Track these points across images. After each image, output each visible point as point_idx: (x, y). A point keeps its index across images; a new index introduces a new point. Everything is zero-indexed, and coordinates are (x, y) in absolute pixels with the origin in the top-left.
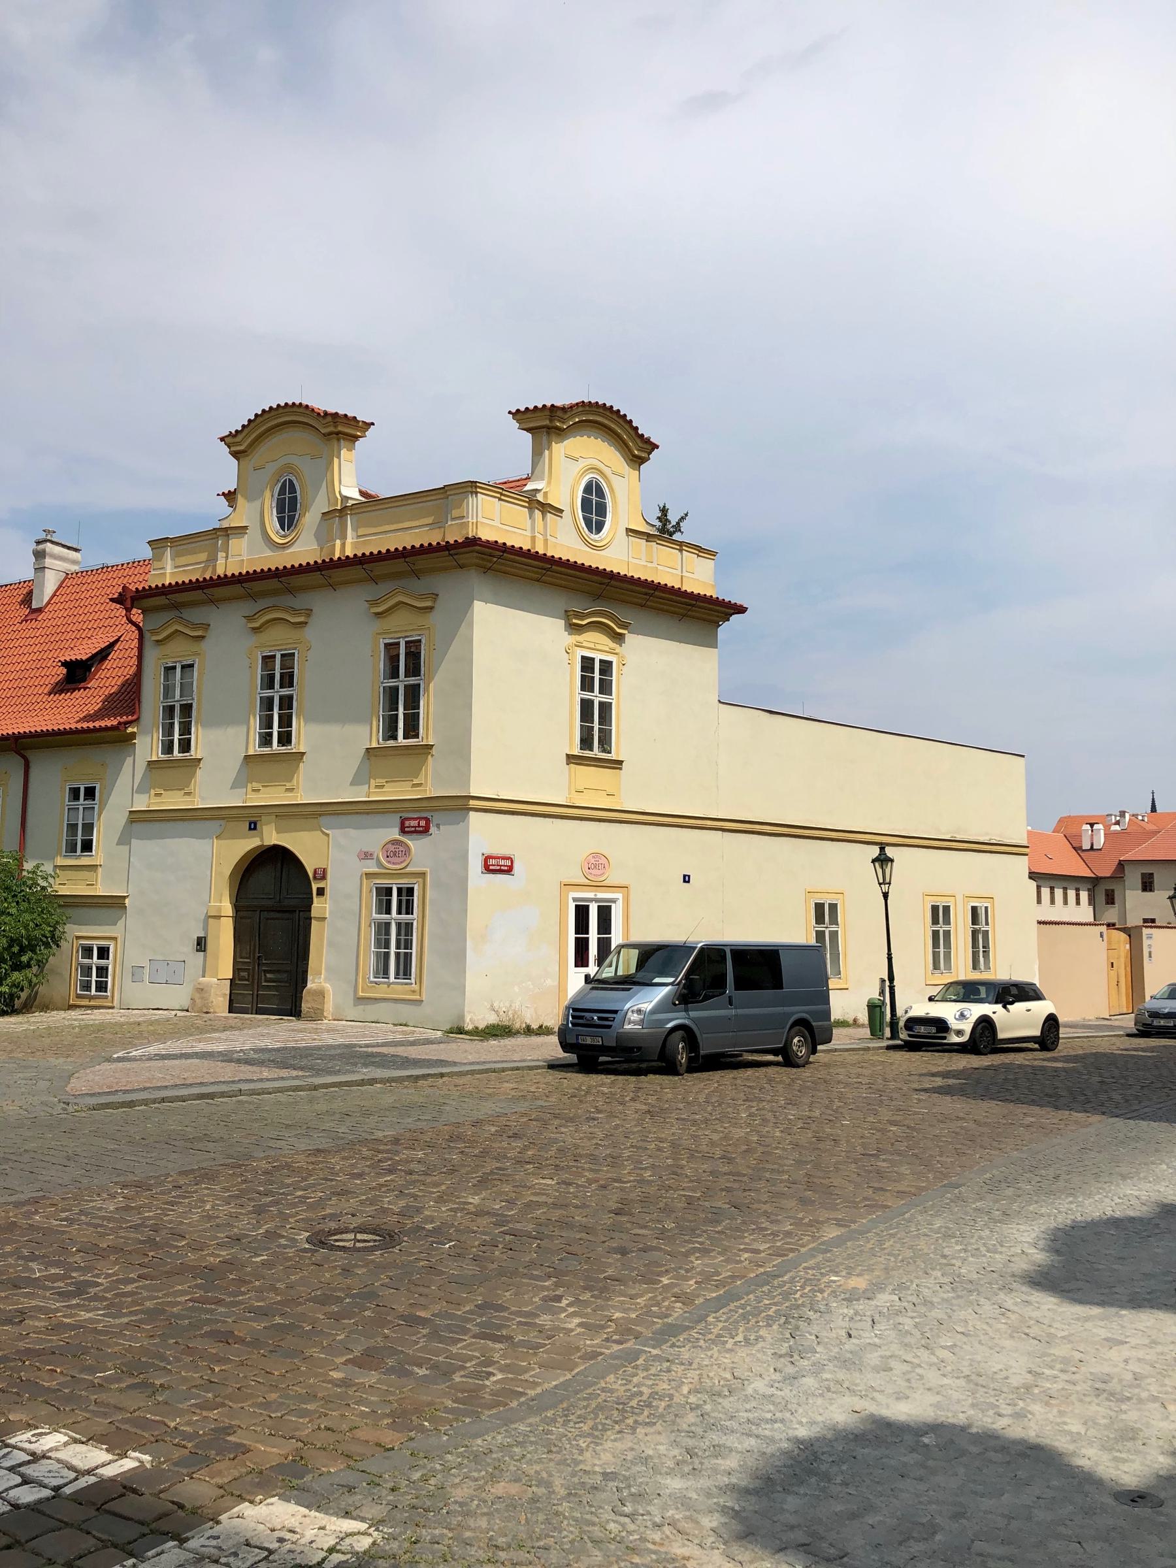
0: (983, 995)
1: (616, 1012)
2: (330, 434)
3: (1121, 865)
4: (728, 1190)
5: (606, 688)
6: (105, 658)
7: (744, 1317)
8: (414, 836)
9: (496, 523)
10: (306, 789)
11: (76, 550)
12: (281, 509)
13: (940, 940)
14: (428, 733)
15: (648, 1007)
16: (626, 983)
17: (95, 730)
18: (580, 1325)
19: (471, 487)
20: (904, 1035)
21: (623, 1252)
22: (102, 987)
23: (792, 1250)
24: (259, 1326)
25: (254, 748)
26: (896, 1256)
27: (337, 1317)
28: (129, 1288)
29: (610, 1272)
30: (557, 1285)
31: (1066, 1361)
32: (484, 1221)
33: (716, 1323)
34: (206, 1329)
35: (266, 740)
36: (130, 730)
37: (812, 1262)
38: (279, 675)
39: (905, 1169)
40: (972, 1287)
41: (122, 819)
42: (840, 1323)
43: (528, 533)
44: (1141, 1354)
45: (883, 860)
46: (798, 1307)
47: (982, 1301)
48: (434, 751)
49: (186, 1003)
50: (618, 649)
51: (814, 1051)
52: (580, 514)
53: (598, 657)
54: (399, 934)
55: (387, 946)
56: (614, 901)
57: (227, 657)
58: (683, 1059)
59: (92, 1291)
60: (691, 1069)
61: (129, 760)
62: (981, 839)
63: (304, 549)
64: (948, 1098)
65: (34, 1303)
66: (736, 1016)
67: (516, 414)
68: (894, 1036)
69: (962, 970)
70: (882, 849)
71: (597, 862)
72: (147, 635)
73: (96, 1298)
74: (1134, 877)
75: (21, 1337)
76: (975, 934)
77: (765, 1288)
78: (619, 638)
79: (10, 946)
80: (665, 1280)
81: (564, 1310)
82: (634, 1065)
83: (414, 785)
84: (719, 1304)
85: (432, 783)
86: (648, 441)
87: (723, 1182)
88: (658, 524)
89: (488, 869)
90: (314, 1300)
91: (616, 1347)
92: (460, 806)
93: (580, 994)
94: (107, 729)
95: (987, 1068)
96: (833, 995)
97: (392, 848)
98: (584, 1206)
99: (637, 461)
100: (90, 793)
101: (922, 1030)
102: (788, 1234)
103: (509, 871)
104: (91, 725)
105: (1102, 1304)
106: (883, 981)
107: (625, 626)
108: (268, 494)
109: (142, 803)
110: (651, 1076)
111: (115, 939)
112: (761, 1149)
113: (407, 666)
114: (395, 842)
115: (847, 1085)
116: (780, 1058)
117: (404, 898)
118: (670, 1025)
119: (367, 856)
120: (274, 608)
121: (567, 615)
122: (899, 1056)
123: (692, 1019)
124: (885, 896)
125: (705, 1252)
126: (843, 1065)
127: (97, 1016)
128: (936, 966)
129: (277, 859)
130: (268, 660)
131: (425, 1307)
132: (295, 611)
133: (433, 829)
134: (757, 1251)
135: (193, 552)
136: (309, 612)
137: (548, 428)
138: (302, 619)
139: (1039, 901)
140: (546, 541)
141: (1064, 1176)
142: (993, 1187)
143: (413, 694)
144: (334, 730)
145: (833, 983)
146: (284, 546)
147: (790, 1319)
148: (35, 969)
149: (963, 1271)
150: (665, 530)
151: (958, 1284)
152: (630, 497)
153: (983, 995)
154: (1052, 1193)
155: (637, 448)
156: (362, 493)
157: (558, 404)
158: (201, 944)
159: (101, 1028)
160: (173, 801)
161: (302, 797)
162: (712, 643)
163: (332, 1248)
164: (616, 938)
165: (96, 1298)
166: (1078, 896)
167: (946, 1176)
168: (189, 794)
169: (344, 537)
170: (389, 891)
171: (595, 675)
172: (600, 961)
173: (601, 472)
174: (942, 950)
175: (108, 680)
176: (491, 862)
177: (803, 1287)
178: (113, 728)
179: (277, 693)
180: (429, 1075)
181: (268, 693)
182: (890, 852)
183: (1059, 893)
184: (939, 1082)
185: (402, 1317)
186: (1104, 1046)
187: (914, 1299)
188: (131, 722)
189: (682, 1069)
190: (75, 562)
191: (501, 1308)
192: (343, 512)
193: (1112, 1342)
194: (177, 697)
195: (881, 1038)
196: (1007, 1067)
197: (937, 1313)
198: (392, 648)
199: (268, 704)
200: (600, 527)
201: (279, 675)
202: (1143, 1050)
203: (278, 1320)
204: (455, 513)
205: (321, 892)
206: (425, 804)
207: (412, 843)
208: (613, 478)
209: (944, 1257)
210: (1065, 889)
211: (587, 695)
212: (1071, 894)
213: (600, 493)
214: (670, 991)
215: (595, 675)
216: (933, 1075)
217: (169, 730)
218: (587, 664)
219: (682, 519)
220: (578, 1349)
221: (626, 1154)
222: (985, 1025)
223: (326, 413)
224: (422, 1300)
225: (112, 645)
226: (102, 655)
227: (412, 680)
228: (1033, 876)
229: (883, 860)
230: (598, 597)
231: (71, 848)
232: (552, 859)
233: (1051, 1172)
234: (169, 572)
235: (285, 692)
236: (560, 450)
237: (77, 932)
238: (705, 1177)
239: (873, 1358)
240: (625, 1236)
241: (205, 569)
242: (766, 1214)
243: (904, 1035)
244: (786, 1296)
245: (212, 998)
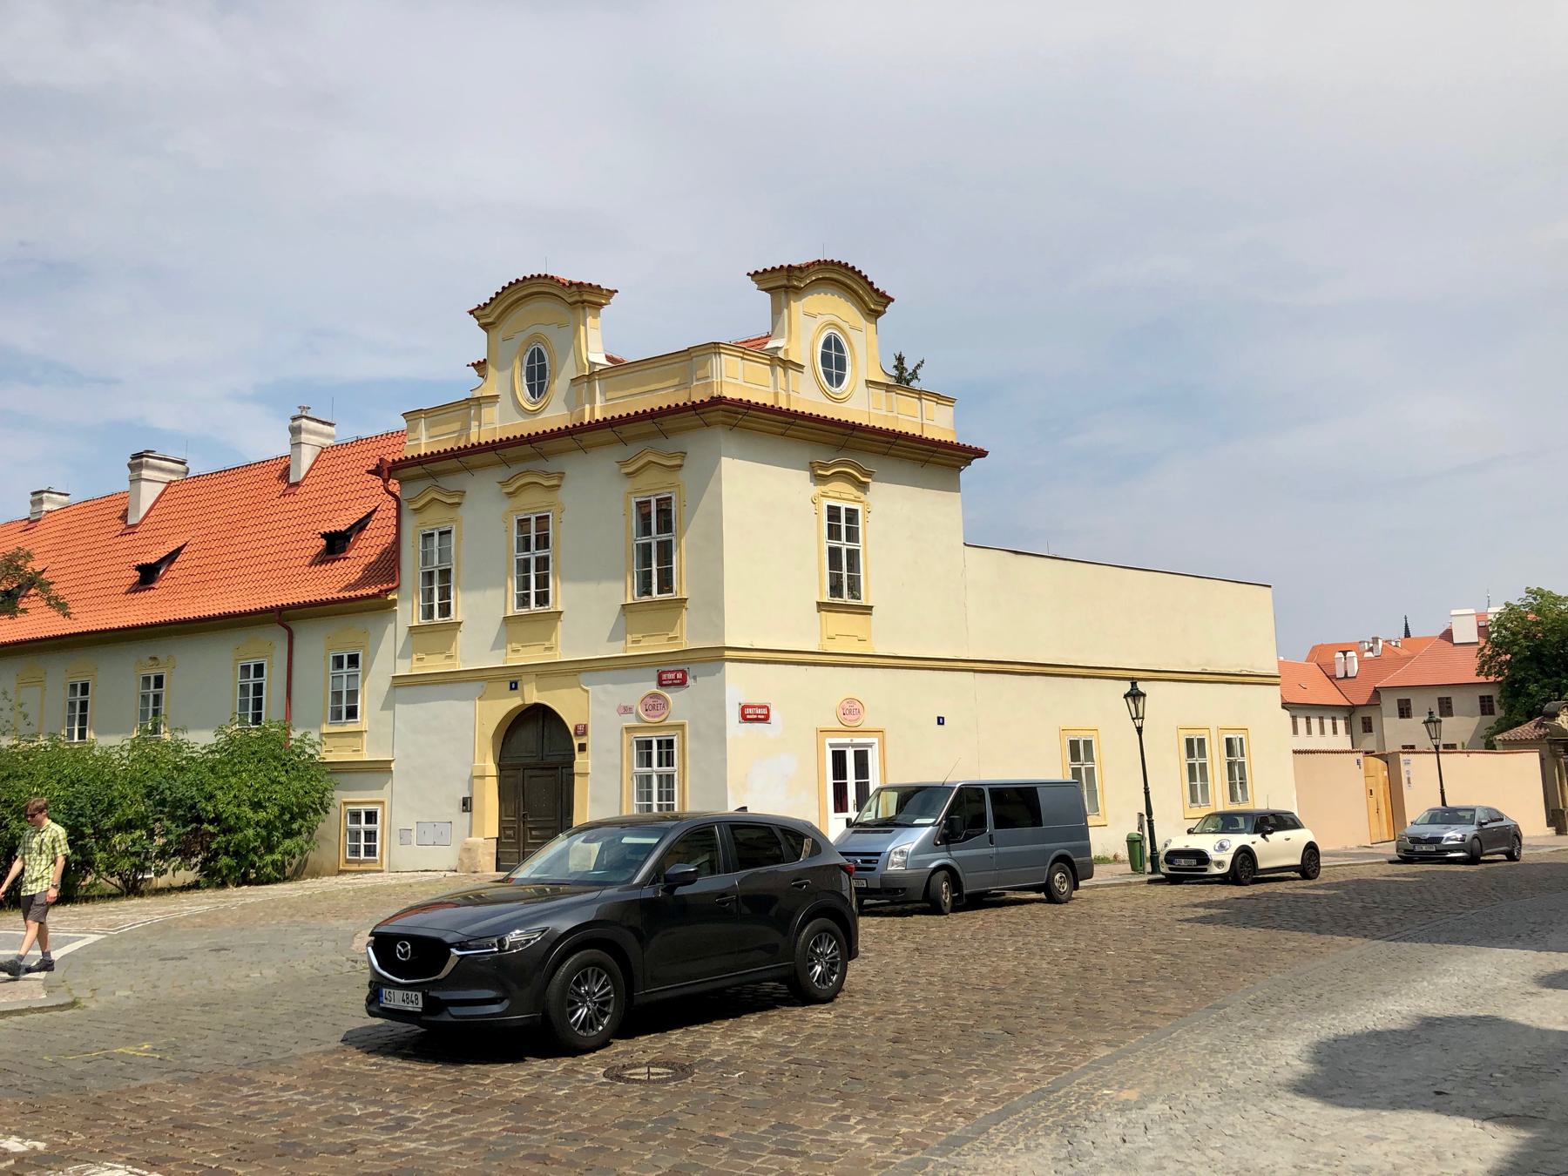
0: (1242, 826)
1: (879, 854)
2: (576, 302)
3: (1377, 692)
4: (999, 1017)
5: (852, 535)
6: (363, 528)
7: (1023, 1127)
9: (740, 382)
10: (564, 647)
11: (330, 424)
12: (530, 377)
13: (1196, 773)
14: (681, 588)
15: (909, 848)
16: (887, 825)
17: (357, 598)
18: (870, 1139)
19: (715, 348)
20: (1164, 868)
21: (904, 1075)
22: (370, 851)
23: (1065, 1069)
24: (572, 1149)
25: (513, 610)
26: (1165, 1071)
27: (642, 1140)
28: (445, 1121)
29: (893, 1093)
30: (844, 1107)
31: (1329, 1156)
32: (772, 1052)
33: (998, 1134)
34: (522, 1153)
35: (524, 601)
36: (390, 597)
37: (1085, 1079)
38: (535, 537)
39: (1170, 994)
40: (1238, 1095)
41: (385, 685)
42: (1114, 1129)
43: (771, 390)
44: (1400, 1148)
45: (1135, 695)
46: (1073, 1118)
47: (1249, 1107)
48: (688, 604)
49: (454, 863)
51: (1076, 887)
53: (843, 505)
54: (660, 786)
55: (649, 798)
56: (870, 745)
57: (484, 520)
58: (947, 898)
59: (412, 1125)
60: (955, 909)
61: (391, 627)
63: (554, 415)
64: (1211, 927)
65: (360, 1136)
66: (997, 854)
67: (755, 275)
68: (1155, 869)
69: (1220, 801)
70: (1134, 684)
71: (851, 708)
72: (404, 504)
73: (415, 1131)
74: (1390, 704)
75: (357, 1164)
76: (1230, 765)
77: (1042, 1103)
78: (863, 487)
79: (282, 814)
80: (946, 1099)
81: (852, 1127)
82: (899, 907)
83: (671, 639)
84: (1000, 1117)
85: (687, 636)
86: (883, 295)
87: (995, 1010)
88: (894, 372)
89: (745, 718)
90: (619, 1126)
91: (905, 1158)
92: (715, 657)
93: (843, 838)
94: (368, 597)
95: (1249, 898)
96: (1093, 834)
97: (650, 701)
98: (862, 1036)
99: (874, 315)
100: (353, 660)
101: (1183, 862)
102: (1060, 1055)
103: (765, 719)
104: (352, 594)
105: (1363, 1107)
107: (868, 474)
108: (517, 364)
109: (404, 668)
110: (916, 917)
111: (382, 803)
112: (1029, 980)
113: (658, 524)
114: (654, 696)
115: (1111, 918)
116: (1042, 896)
117: (664, 751)
118: (933, 865)
119: (627, 710)
120: (528, 471)
121: (812, 467)
122: (1159, 888)
124: (1139, 730)
125: (984, 1073)
126: (1106, 900)
127: (367, 880)
128: (1194, 799)
129: (540, 716)
130: (523, 523)
131: (720, 1129)
132: (548, 475)
133: (690, 681)
134: (1033, 1071)
135: (447, 422)
136: (561, 475)
137: (786, 287)
138: (554, 482)
139: (1295, 731)
140: (789, 396)
141: (1326, 995)
142: (1256, 1007)
143: (666, 551)
144: (590, 588)
145: (1091, 820)
146: (534, 413)
147: (1067, 1129)
148: (305, 835)
149: (1230, 1082)
150: (902, 379)
151: (1225, 1093)
153: (1242, 826)
154: (1313, 1010)
155: (873, 301)
156: (609, 358)
157: (794, 264)
158: (467, 805)
159: (374, 890)
160: (532, 655)
162: (955, 487)
163: (628, 1081)
164: (874, 782)
165: (415, 1131)
166: (1334, 725)
167: (1211, 998)
168: (550, 649)
169: (592, 402)
170: (649, 744)
171: (842, 524)
172: (860, 806)
174: (1198, 783)
175: (366, 550)
177: (1077, 1101)
178: (374, 596)
179: (533, 555)
181: (524, 555)
182: (1141, 686)
183: (1315, 722)
184: (1201, 912)
185: (702, 1138)
186: (1366, 873)
187: (1184, 1107)
188: (391, 590)
189: (947, 909)
190: (329, 436)
191: (794, 1128)
192: (590, 377)
193: (1372, 1139)
194: (436, 563)
195: (1142, 872)
196: (1269, 896)
197: (1207, 1119)
198: (643, 506)
199: (524, 566)
200: (840, 379)
201: (535, 537)
202: (1405, 875)
203: (588, 1144)
204: (700, 373)
205: (582, 748)
206: (680, 657)
207: (670, 696)
208: (851, 333)
209: (1212, 1070)
210: (1321, 718)
211: (835, 543)
212: (1328, 723)
213: (839, 347)
214: (929, 835)
215: (842, 524)
216: (1196, 906)
217: (429, 596)
218: (833, 513)
220: (870, 1160)
221: (898, 988)
222: (1245, 853)
223: (571, 284)
224: (719, 1123)
225: (370, 515)
226: (361, 525)
227: (664, 537)
228: (1285, 706)
229: (1135, 695)
230: (841, 448)
231: (337, 715)
232: (807, 706)
233: (1314, 992)
234: (424, 442)
235: (541, 553)
237: (346, 798)
238: (976, 1006)
239: (1147, 1159)
240: (904, 1062)
241: (458, 438)
242: (1039, 1039)
243: (1164, 868)
244: (1062, 1109)
245: (480, 857)
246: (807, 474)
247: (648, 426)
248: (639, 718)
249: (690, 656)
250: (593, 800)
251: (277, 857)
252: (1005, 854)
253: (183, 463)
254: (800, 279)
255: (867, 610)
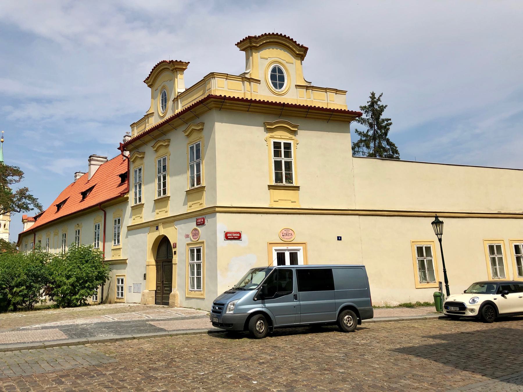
5: (288, 154)
8: (200, 226)
19: (212, 75)
25: (157, 197)
43: (243, 92)
50: (294, 137)
51: (359, 323)
52: (270, 81)
53: (282, 142)
56: (299, 250)
62: (517, 212)
70: (437, 217)
71: (287, 233)
78: (294, 133)
85: (205, 202)
89: (227, 238)
92: (212, 211)
97: (194, 232)
101: (452, 309)
103: (239, 238)
106: (440, 283)
119: (187, 236)
121: (265, 124)
122: (444, 322)
123: (267, 308)
124: (440, 240)
136: (169, 140)
152: (295, 71)
155: (300, 52)
160: (162, 215)
161: (170, 214)
173: (280, 63)
174: (498, 267)
176: (229, 235)
180: (124, 339)
205: (175, 253)
208: (287, 65)
213: (280, 71)
218: (277, 145)
219: (380, 96)
230: (280, 115)
236: (257, 56)
237: (114, 274)
246: (262, 129)
247: (189, 115)
248: (191, 240)
249: (206, 211)
250: (178, 275)
251: (77, 296)
252: (304, 305)
253: (106, 158)
254: (257, 43)
255: (297, 188)
